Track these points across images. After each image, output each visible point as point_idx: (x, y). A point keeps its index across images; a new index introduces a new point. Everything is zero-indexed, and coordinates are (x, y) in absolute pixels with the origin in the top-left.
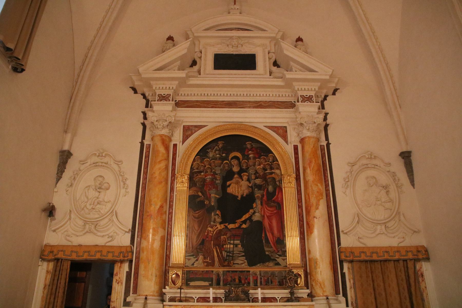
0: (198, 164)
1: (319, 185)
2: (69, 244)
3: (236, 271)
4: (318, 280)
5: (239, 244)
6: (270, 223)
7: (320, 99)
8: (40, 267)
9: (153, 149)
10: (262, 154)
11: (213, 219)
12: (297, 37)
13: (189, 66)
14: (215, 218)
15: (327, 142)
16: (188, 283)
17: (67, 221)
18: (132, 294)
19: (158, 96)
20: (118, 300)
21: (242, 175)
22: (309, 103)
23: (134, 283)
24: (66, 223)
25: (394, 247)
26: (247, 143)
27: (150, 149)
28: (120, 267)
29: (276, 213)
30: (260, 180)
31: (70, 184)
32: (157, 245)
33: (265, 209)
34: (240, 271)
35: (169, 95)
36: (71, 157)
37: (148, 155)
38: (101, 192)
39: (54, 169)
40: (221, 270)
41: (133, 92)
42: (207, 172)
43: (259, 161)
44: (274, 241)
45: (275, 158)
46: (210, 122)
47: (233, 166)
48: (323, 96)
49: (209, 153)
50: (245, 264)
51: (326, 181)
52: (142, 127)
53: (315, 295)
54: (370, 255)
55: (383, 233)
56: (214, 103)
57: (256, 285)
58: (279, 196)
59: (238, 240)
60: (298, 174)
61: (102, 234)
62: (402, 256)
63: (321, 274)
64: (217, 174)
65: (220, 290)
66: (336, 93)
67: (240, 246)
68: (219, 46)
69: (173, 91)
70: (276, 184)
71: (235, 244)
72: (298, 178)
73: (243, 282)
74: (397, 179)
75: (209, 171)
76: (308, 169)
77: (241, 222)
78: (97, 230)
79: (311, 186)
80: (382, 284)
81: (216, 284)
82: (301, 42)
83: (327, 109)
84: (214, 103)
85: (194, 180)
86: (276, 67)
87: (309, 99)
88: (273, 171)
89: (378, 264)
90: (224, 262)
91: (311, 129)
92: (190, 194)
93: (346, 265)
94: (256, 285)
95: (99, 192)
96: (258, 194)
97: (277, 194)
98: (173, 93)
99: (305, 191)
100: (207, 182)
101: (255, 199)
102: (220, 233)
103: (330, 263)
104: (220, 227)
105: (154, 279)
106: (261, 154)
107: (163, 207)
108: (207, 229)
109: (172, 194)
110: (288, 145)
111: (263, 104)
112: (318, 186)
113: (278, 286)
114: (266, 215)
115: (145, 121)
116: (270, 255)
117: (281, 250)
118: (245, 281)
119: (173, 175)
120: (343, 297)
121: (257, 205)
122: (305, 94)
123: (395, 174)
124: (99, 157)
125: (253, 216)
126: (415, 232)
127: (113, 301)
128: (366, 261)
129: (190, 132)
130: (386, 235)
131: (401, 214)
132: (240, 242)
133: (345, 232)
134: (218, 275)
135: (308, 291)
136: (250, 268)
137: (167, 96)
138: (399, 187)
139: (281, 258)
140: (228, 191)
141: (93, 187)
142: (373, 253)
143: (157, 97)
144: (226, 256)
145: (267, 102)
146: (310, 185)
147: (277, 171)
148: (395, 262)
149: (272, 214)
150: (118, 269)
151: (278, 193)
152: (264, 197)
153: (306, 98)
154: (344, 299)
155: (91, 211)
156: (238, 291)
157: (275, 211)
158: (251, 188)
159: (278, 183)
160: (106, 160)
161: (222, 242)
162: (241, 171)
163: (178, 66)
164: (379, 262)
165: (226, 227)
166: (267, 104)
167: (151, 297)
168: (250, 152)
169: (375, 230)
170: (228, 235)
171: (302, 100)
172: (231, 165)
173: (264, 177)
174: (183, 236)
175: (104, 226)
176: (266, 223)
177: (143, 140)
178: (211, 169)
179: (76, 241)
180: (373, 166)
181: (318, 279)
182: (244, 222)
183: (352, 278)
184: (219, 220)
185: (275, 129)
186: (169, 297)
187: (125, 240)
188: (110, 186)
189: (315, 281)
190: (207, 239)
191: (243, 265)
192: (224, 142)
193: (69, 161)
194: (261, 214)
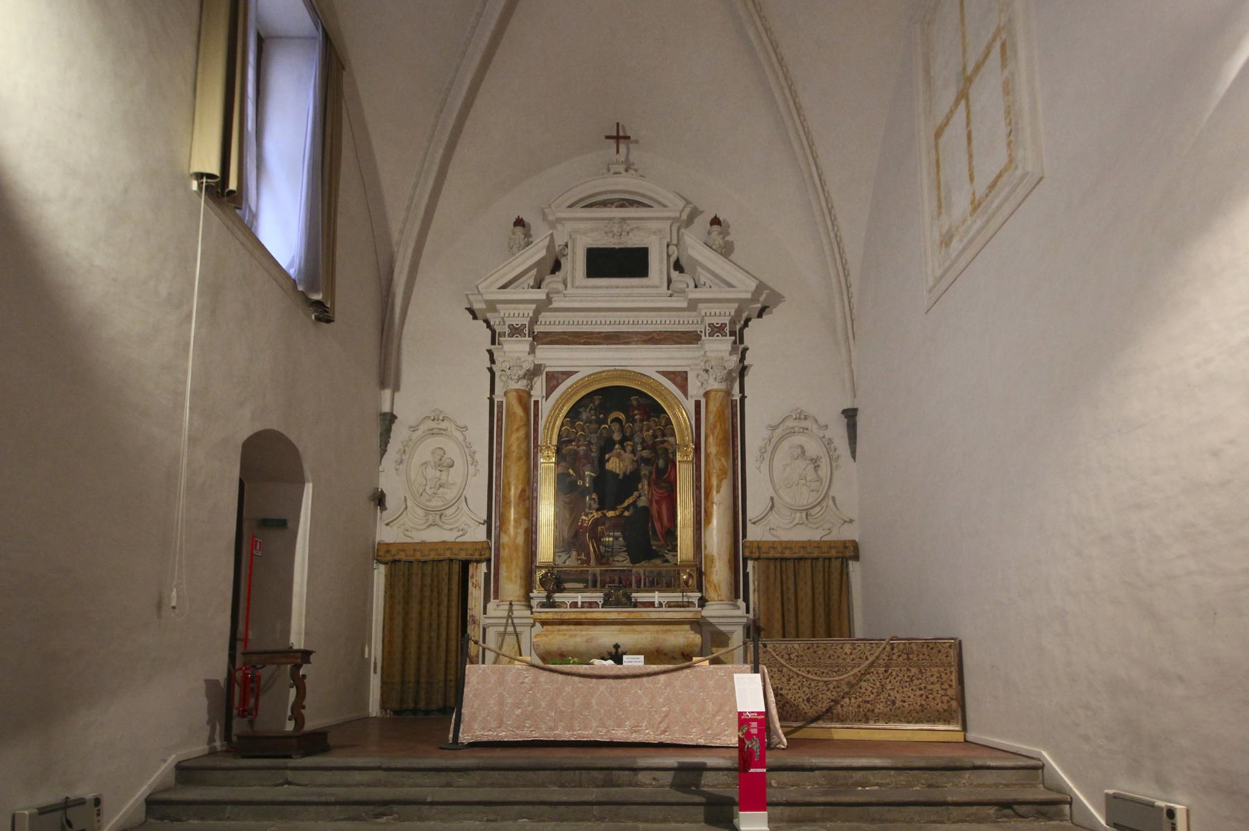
1: (723, 459)
2: (409, 540)
7: (738, 327)
8: (376, 571)
9: (507, 411)
10: (652, 414)
11: (588, 505)
12: (713, 216)
13: (549, 272)
14: (590, 504)
17: (403, 511)
22: (720, 337)
23: (494, 586)
24: (402, 513)
25: (815, 541)
26: (632, 398)
28: (477, 567)
31: (399, 461)
32: (520, 540)
33: (654, 491)
34: (620, 570)
36: (396, 421)
39: (376, 441)
40: (598, 570)
41: (471, 316)
42: (580, 441)
47: (614, 432)
48: (742, 322)
51: (734, 452)
52: (488, 374)
55: (802, 524)
56: (585, 336)
57: (639, 586)
59: (618, 532)
61: (450, 527)
62: (823, 553)
64: (592, 444)
66: (764, 313)
67: (621, 539)
70: (669, 457)
72: (697, 450)
74: (833, 448)
76: (711, 437)
78: (442, 522)
82: (717, 226)
83: (747, 342)
88: (666, 439)
90: (601, 559)
93: (750, 564)
94: (639, 586)
95: (441, 471)
96: (645, 471)
97: (669, 470)
102: (596, 523)
104: (596, 515)
105: (519, 581)
109: (535, 472)
115: (493, 366)
116: (658, 550)
117: (671, 544)
119: (536, 446)
121: (644, 486)
122: (715, 321)
124: (436, 421)
126: (845, 522)
128: (776, 559)
133: (753, 521)
134: (594, 575)
135: (699, 595)
137: (522, 328)
139: (670, 553)
140: (607, 468)
141: (432, 464)
142: (786, 548)
147: (671, 439)
149: (660, 497)
151: (671, 469)
155: (433, 497)
157: (666, 494)
159: (671, 456)
160: (443, 425)
162: (622, 442)
163: (533, 278)
164: (792, 561)
165: (604, 514)
166: (662, 337)
167: (517, 603)
170: (607, 525)
172: (611, 430)
173: (653, 448)
176: (654, 507)
178: (585, 437)
182: (627, 508)
184: (596, 506)
185: (672, 376)
187: (479, 534)
188: (453, 462)
191: (625, 562)
193: (394, 427)
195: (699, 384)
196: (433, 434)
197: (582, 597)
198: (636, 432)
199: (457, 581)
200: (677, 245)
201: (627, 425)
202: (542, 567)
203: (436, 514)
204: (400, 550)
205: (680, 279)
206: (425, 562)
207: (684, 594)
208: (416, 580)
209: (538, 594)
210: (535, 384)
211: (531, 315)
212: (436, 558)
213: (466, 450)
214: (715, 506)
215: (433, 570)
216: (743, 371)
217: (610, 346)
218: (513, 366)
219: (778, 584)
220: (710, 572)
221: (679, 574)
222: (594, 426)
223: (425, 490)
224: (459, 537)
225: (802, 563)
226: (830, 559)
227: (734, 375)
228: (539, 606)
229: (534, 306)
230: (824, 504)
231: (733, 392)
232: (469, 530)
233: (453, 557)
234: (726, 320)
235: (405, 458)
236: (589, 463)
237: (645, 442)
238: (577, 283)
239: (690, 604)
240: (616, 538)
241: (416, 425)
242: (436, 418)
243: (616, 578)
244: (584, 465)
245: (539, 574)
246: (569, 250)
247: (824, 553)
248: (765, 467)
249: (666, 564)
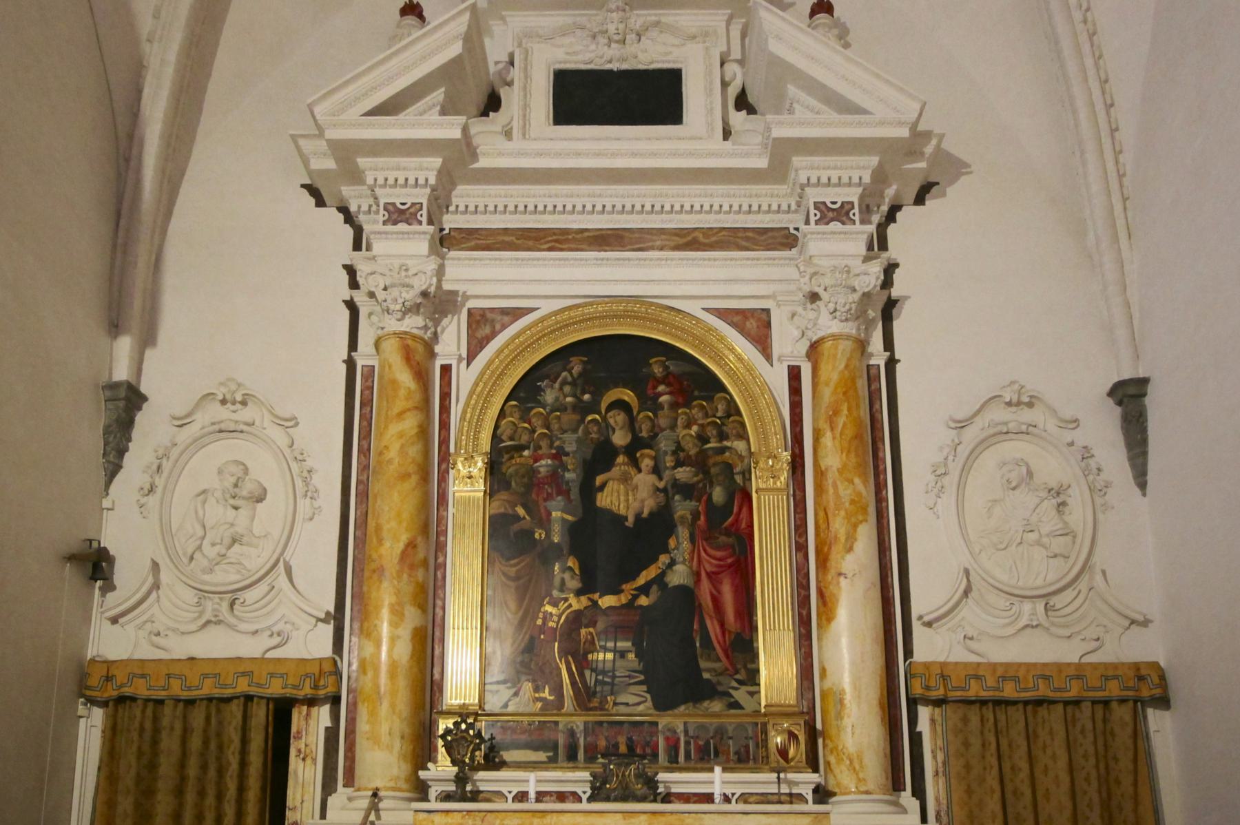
0: (514, 424)
1: (857, 481)
3: (621, 723)
4: (845, 750)
5: (631, 651)
6: (715, 592)
8: (82, 721)
9: (381, 377)
10: (696, 393)
11: (557, 581)
14: (563, 581)
15: (888, 354)
16: (547, 687)
18: (344, 786)
19: (385, 209)
20: (304, 804)
21: (638, 455)
25: (1069, 664)
27: (373, 381)
28: (308, 715)
29: (730, 566)
30: (688, 469)
31: (147, 486)
32: (404, 651)
33: (703, 554)
35: (418, 206)
36: (145, 406)
37: (370, 397)
38: (240, 508)
39: (92, 440)
40: (579, 722)
41: (312, 201)
42: (540, 448)
43: (685, 413)
44: (725, 641)
45: (732, 404)
46: (546, 297)
48: (885, 208)
49: (544, 391)
50: (647, 704)
52: (346, 313)
53: (836, 790)
54: (995, 685)
55: (1037, 626)
56: (555, 237)
57: (673, 759)
58: (741, 516)
59: (627, 640)
60: (797, 451)
63: (853, 734)
64: (567, 454)
65: (574, 771)
66: (927, 196)
67: (631, 656)
68: (567, 40)
69: (428, 190)
71: (618, 651)
73: (639, 751)
75: (544, 444)
76: (829, 434)
77: (633, 590)
78: (235, 616)
79: (835, 485)
80: (1024, 765)
81: (565, 758)
84: (555, 237)
85: (504, 470)
86: (744, 112)
87: (840, 213)
88: (726, 443)
89: (1018, 710)
91: (843, 310)
92: (493, 512)
93: (924, 713)
94: (673, 759)
95: (236, 508)
96: (682, 508)
97: (735, 509)
98: (429, 200)
99: (816, 503)
100: (539, 476)
101: (675, 526)
102: (576, 620)
103: (881, 704)
104: (577, 604)
105: (397, 744)
106: (693, 391)
107: (415, 547)
108: (542, 610)
110: (772, 366)
111: (701, 239)
112: (853, 484)
113: (735, 764)
114: (705, 570)
116: (714, 680)
117: (745, 667)
118: (644, 750)
119: (445, 457)
120: (914, 799)
121: (681, 542)
123: (1089, 453)
124: (229, 405)
125: (669, 572)
126: (1133, 622)
127: (291, 807)
128: (983, 702)
129: (487, 330)
130: (1048, 629)
131: (1098, 570)
132: (633, 645)
133: (926, 619)
134: (572, 733)
135: (815, 778)
136: (657, 715)
137: (412, 210)
138: (1098, 491)
139: (744, 688)
140: (598, 504)
141: (218, 494)
143: (382, 211)
144: (595, 684)
145: (715, 231)
146: (830, 481)
147: (740, 445)
148: (1070, 709)
150: (303, 723)
152: (699, 519)
153: (833, 210)
154: (915, 804)
156: (627, 773)
157: (729, 561)
158: (663, 494)
159: (738, 479)
160: (246, 414)
161: (582, 644)
162: (632, 451)
165: (595, 603)
166: (714, 239)
168: (661, 388)
169: (1019, 615)
171: (819, 220)
172: (608, 425)
173: (700, 463)
174: (476, 628)
175: (256, 606)
177: (353, 354)
178: (551, 438)
179: (180, 648)
180: (1024, 428)
181: (843, 746)
182: (644, 590)
183: (941, 749)
184: (574, 584)
185: (737, 319)
186: (438, 792)
187: (319, 644)
189: (835, 753)
190: (542, 637)
191: (641, 708)
192: (586, 359)
193: (140, 418)
194: (691, 567)
195: (797, 333)
196: (221, 431)
197: (538, 781)
198: (662, 430)
199: (262, 744)
200: (741, 62)
201: (641, 416)
202: (449, 713)
203: (221, 599)
204: (135, 675)
205: (748, 126)
206: (190, 703)
207: (782, 775)
208: (170, 742)
209: (442, 768)
210: (443, 331)
211: (432, 181)
212: (217, 692)
213: (294, 466)
214: (843, 582)
215: (208, 719)
216: (889, 310)
217: (602, 254)
218: (393, 286)
219: (994, 761)
220: (838, 727)
221: (765, 732)
222: (569, 418)
223: (199, 548)
224: (274, 648)
225: (1043, 711)
226: (1106, 703)
227: (871, 314)
228: (439, 800)
229: (437, 162)
230: (1083, 585)
231: (870, 349)
232: (295, 633)
233: (253, 691)
234: (853, 195)
235: (160, 482)
236: (559, 493)
237: (683, 450)
238: (533, 132)
239: (794, 798)
240: (622, 654)
241: (183, 413)
242: (228, 397)
243: (622, 740)
244: (549, 497)
245: (444, 724)
246: (516, 74)
247: (1094, 689)
248: (947, 502)
249: (733, 711)
